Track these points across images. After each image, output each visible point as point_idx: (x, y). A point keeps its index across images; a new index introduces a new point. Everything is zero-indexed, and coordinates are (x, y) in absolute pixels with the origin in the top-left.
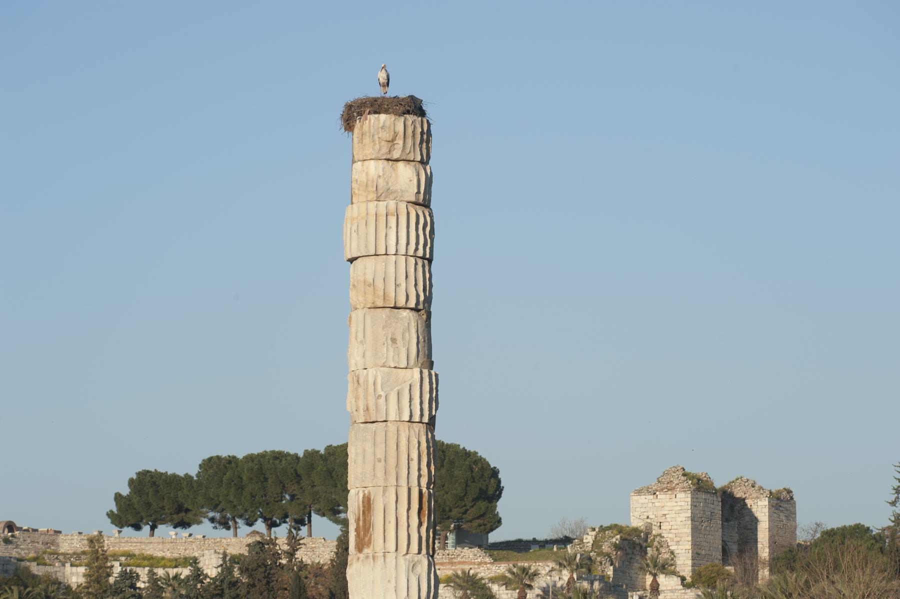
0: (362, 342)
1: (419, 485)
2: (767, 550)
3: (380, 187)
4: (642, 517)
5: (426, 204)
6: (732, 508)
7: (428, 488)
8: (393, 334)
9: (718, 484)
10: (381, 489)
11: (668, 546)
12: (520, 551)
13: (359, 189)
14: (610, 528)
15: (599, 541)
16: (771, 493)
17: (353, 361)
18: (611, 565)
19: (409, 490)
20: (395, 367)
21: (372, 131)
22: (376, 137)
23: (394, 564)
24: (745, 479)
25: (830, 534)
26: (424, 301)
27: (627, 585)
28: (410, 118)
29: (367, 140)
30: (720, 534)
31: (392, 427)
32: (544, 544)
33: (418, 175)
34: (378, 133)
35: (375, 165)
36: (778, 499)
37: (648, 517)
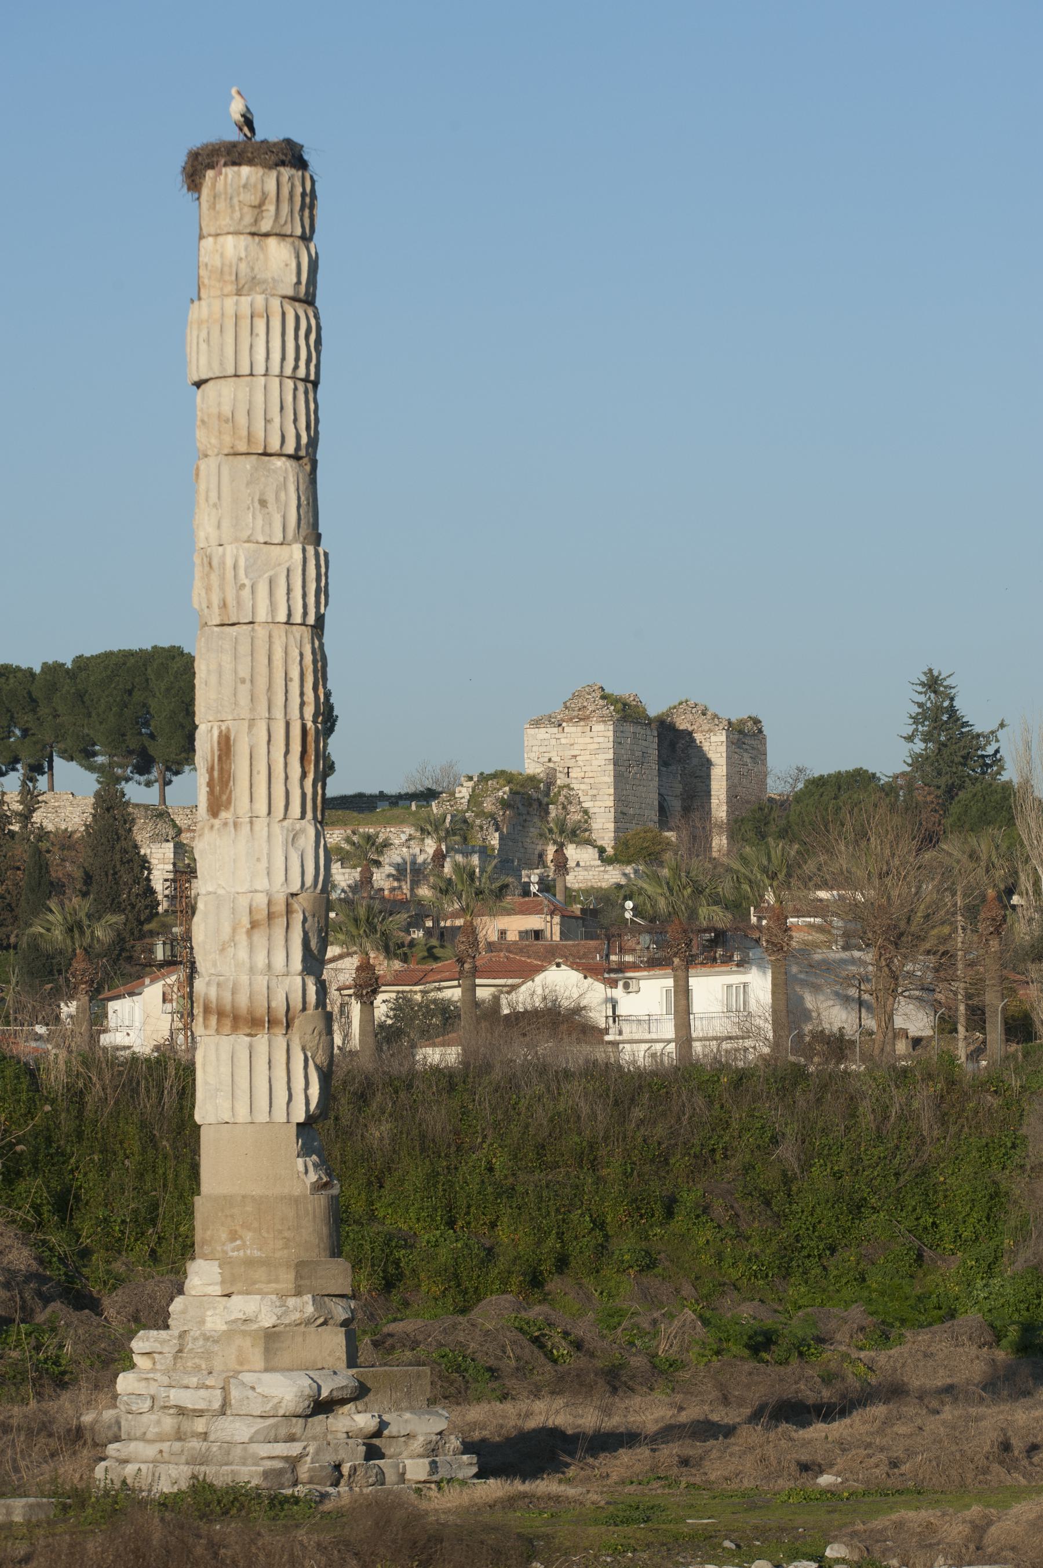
0: (215, 505)
1: (302, 718)
2: (725, 808)
3: (242, 274)
4: (541, 760)
5: (309, 300)
6: (673, 745)
7: (315, 722)
8: (262, 494)
9: (654, 710)
10: (246, 724)
11: (580, 803)
12: (361, 810)
13: (210, 278)
14: (494, 776)
15: (479, 795)
16: (730, 723)
17: (202, 534)
18: (496, 831)
19: (288, 724)
20: (265, 543)
21: (229, 191)
22: (235, 201)
23: (265, 833)
24: (691, 703)
25: (820, 783)
26: (308, 445)
27: (519, 860)
28: (286, 172)
29: (221, 205)
30: (656, 784)
31: (261, 632)
32: (396, 800)
33: (298, 257)
34: (239, 194)
35: (232, 239)
36: (741, 732)
37: (550, 760)
